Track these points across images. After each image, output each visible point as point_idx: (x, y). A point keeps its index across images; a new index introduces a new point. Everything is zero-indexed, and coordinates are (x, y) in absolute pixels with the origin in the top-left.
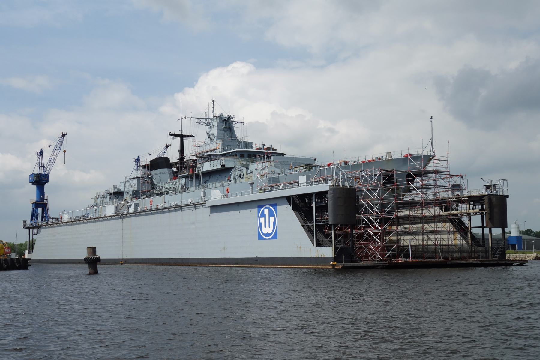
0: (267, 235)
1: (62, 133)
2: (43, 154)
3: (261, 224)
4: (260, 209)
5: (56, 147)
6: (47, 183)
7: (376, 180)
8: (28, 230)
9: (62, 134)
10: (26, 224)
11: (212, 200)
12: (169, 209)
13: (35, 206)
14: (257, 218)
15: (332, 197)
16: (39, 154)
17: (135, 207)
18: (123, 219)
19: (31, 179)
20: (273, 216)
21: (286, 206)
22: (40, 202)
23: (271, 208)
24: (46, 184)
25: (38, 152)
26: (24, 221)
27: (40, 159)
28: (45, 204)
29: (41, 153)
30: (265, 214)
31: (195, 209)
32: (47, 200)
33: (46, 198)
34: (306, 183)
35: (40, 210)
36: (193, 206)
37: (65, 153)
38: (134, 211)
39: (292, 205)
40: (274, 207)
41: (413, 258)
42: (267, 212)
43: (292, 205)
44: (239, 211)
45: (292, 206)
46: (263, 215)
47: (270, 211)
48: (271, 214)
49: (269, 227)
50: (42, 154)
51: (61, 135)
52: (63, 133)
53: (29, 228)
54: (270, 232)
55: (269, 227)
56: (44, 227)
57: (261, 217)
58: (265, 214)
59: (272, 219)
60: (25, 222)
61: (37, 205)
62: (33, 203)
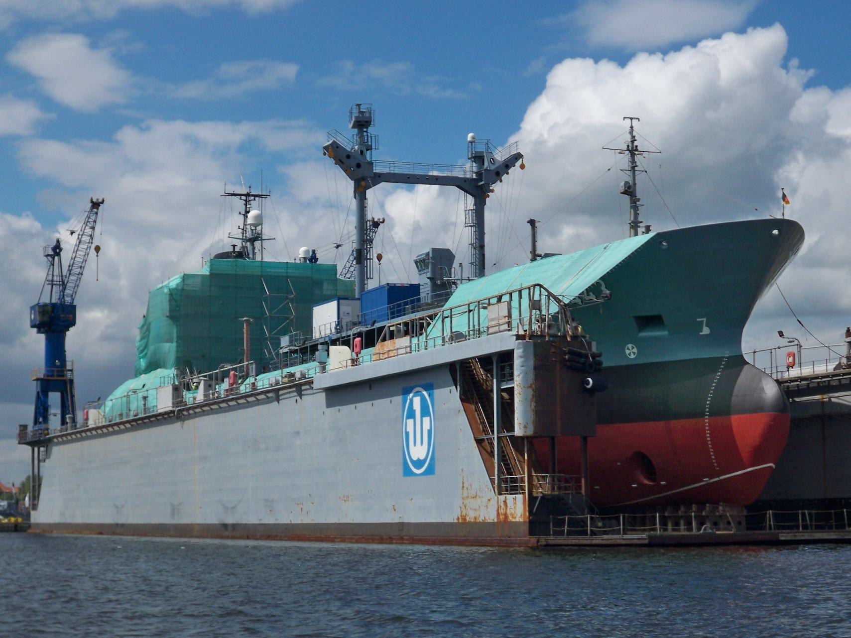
0: (419, 463)
1: (90, 201)
2: (62, 253)
3: (407, 434)
4: (405, 396)
5: (80, 237)
6: (70, 329)
7: (396, 309)
8: (29, 448)
9: (92, 202)
10: (47, 429)
11: (329, 372)
12: (257, 397)
13: (42, 387)
14: (401, 420)
15: (522, 366)
16: (51, 253)
17: (205, 391)
18: (183, 420)
19: (33, 317)
20: (428, 414)
21: (448, 389)
22: (52, 376)
23: (425, 393)
24: (68, 330)
25: (420, 274)
26: (21, 426)
27: (53, 265)
28: (65, 382)
29: (58, 251)
30: (415, 410)
31: (301, 396)
32: (71, 370)
33: (69, 367)
34: (507, 325)
35: (54, 397)
36: (294, 389)
37: (97, 252)
38: (202, 401)
39: (458, 387)
40: (431, 392)
41: (798, 513)
42: (417, 401)
43: (458, 387)
44: (370, 403)
45: (459, 389)
46: (411, 415)
47: (423, 401)
48: (425, 412)
49: (422, 444)
50: (58, 254)
51: (90, 205)
52: (94, 200)
53: (32, 444)
54: (422, 457)
55: (422, 444)
56: (55, 440)
57: (409, 417)
58: (415, 410)
59: (426, 420)
60: (24, 428)
61: (46, 385)
62: (37, 380)
